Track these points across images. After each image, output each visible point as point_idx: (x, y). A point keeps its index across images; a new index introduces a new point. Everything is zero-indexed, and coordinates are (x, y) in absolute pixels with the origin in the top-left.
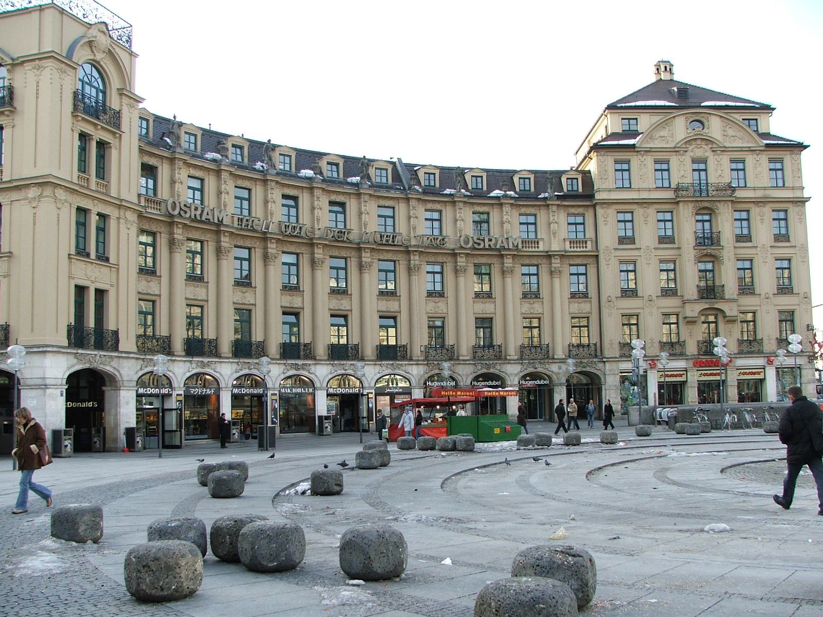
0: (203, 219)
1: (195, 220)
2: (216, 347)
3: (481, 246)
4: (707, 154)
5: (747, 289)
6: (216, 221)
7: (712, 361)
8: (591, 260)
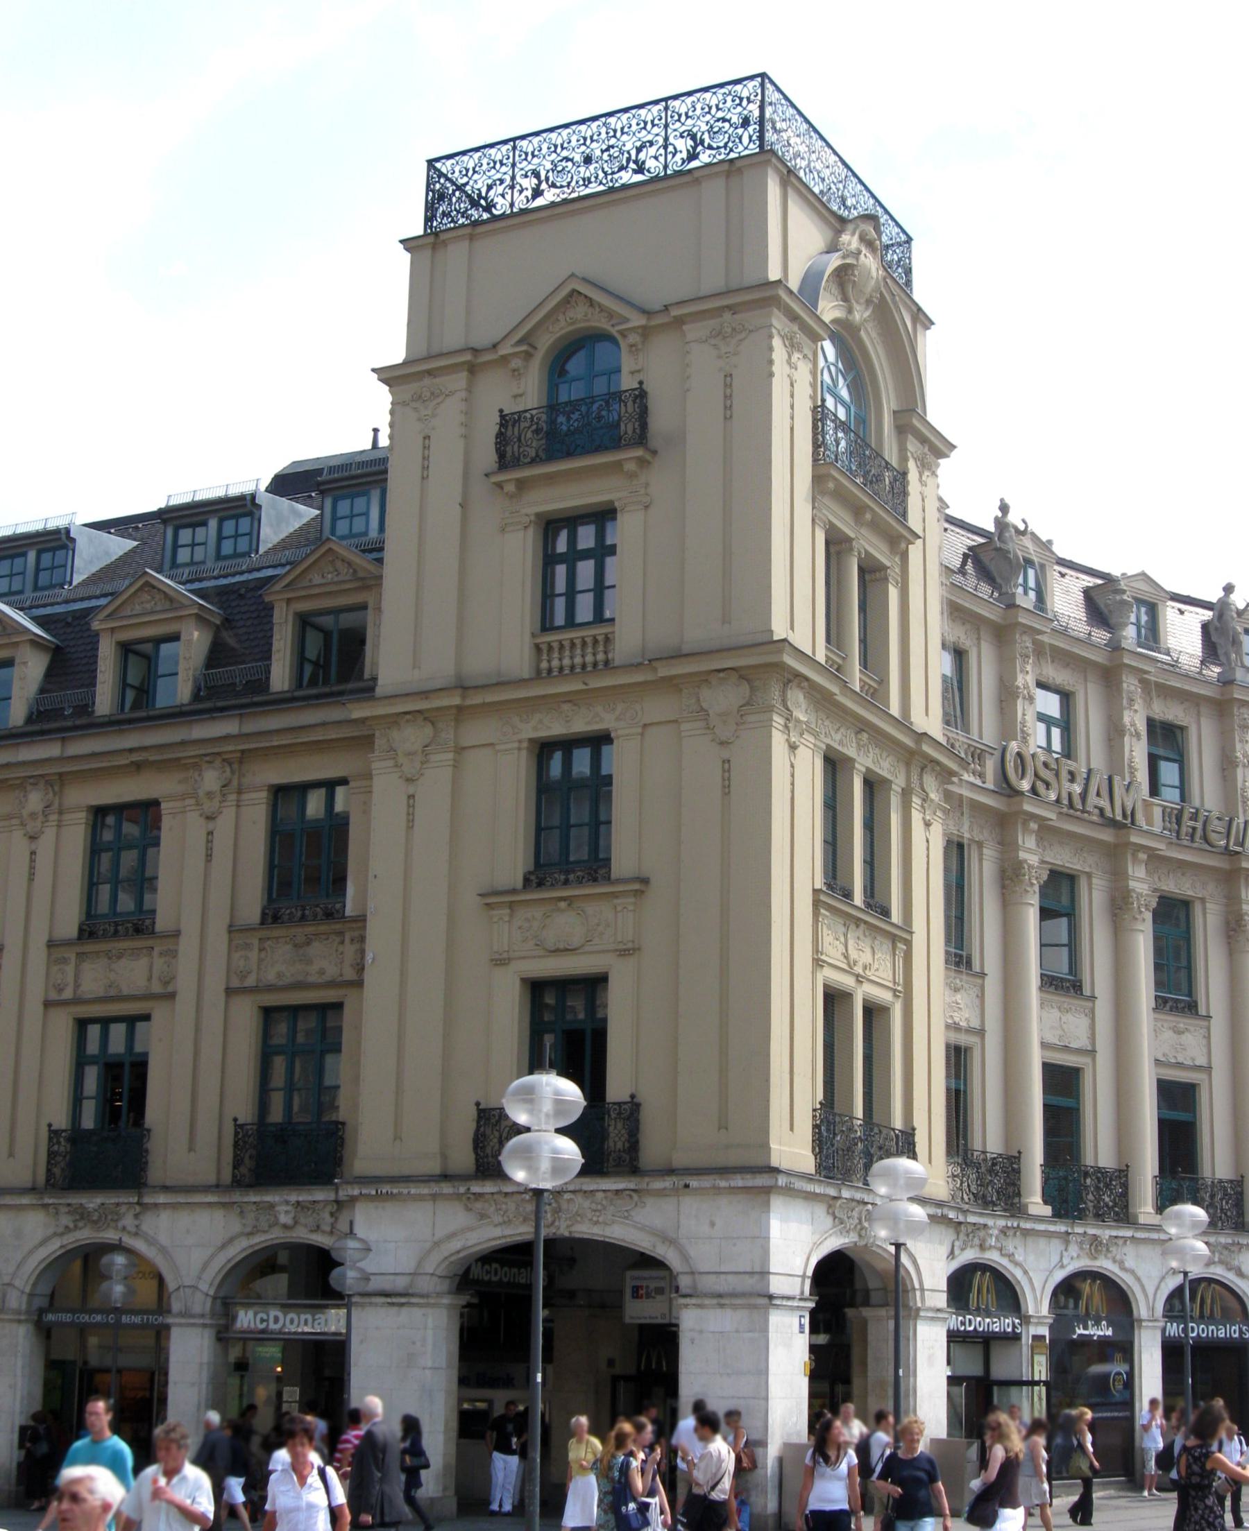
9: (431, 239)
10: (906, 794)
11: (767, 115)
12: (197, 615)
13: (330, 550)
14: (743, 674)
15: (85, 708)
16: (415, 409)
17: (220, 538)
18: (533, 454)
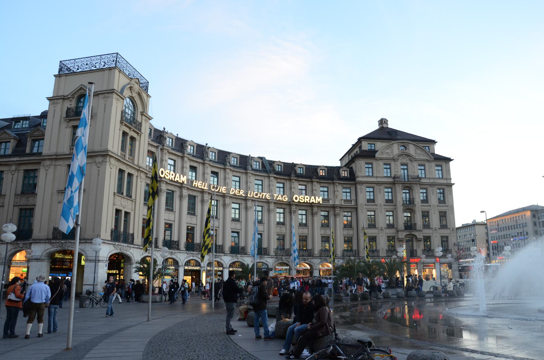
0: (176, 180)
1: (172, 181)
2: (178, 245)
4: (407, 162)
5: (427, 226)
8: (354, 210)
9: (59, 75)
10: (137, 176)
11: (117, 60)
12: (14, 138)
13: (38, 129)
14: (103, 156)
16: (104, 99)
17: (23, 124)
18: (72, 115)
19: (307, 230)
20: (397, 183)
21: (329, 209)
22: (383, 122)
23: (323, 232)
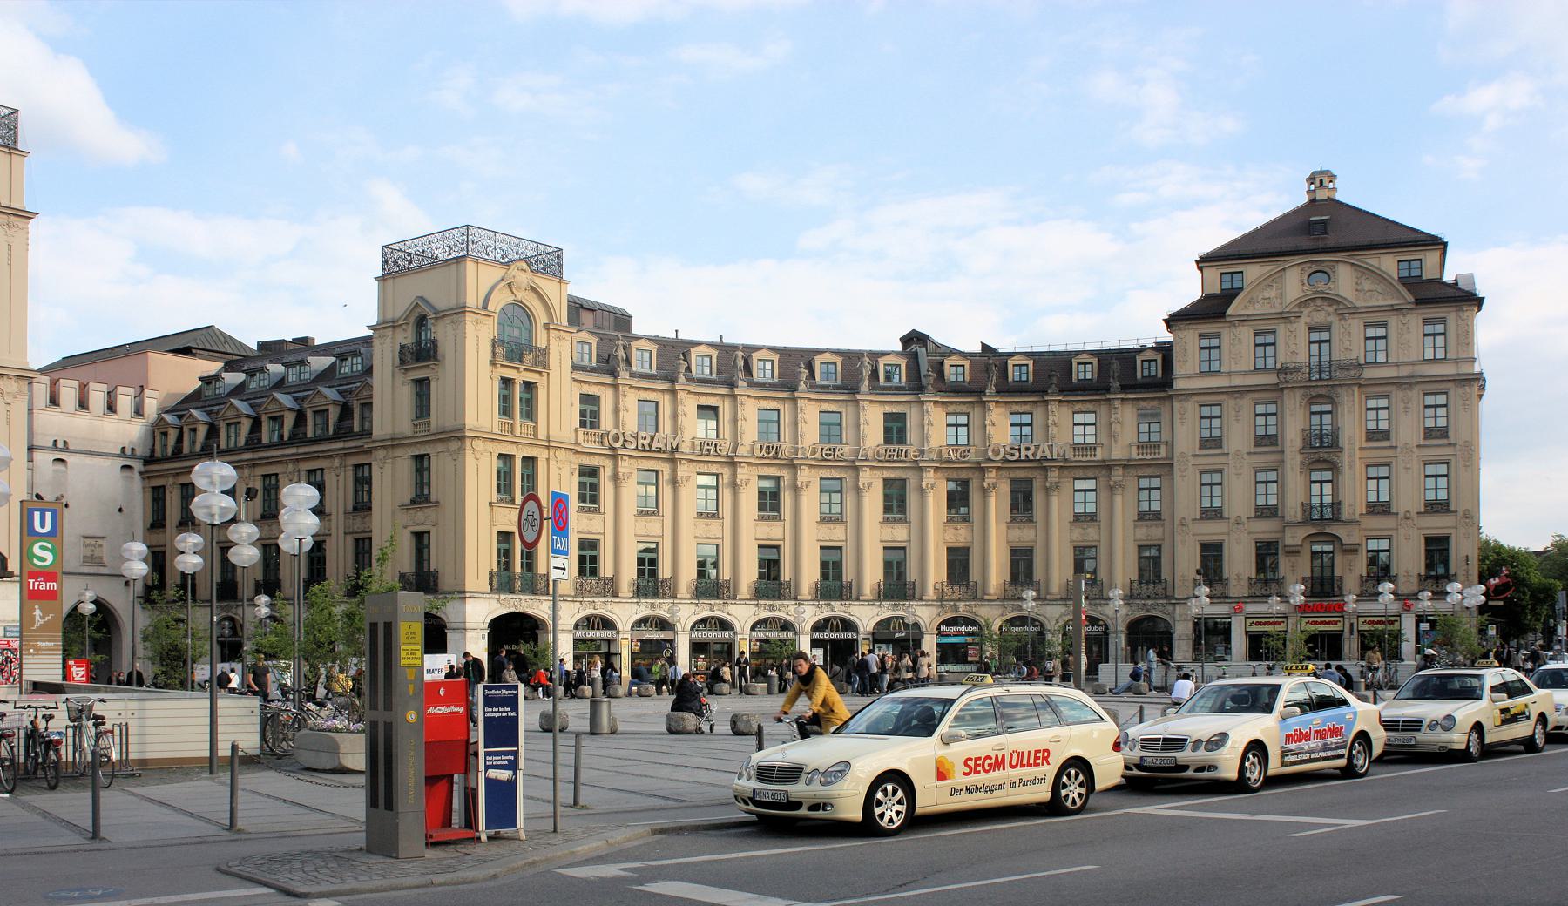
3: (1014, 458)
4: (1330, 319)
6: (669, 449)
7: (1322, 606)
15: (260, 440)
19: (1032, 532)
20: (1287, 388)
21: (1097, 472)
22: (1319, 179)
23: (1077, 534)
